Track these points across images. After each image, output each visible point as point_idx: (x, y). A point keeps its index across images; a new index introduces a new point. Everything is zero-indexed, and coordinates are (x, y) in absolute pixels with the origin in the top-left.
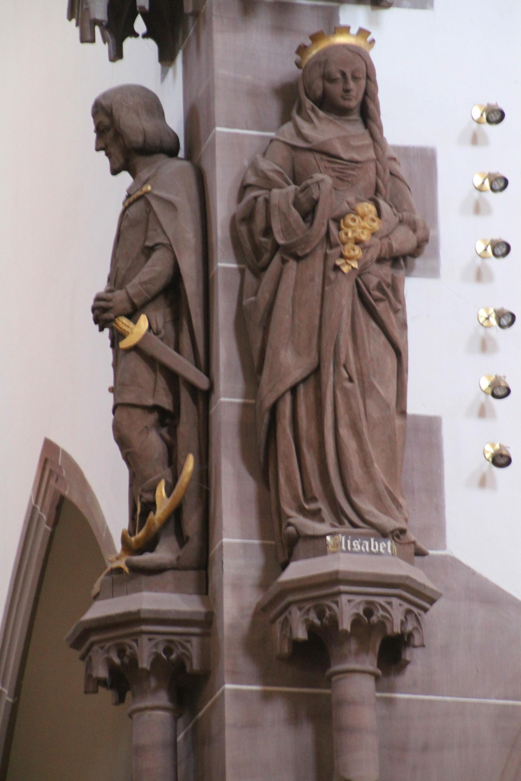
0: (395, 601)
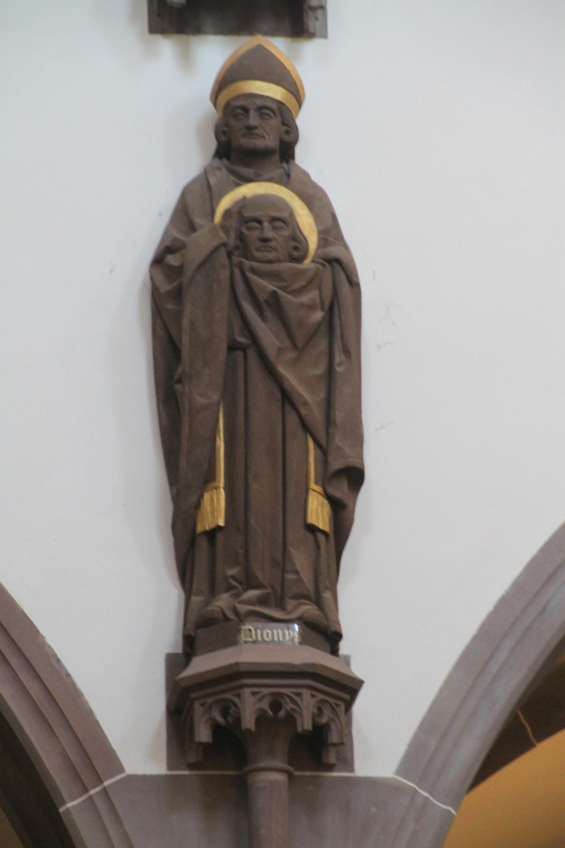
0: (306, 693)
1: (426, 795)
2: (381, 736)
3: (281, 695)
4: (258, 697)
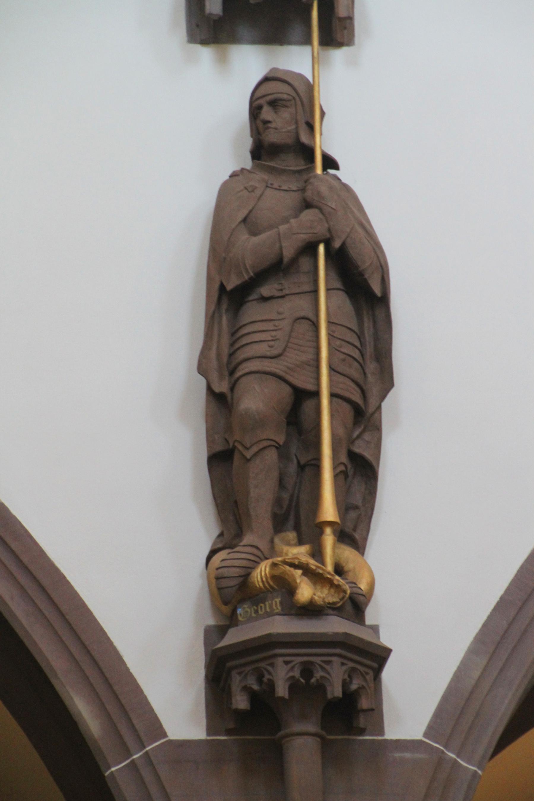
1: (454, 756)
2: (410, 701)
3: (312, 663)
4: (290, 665)
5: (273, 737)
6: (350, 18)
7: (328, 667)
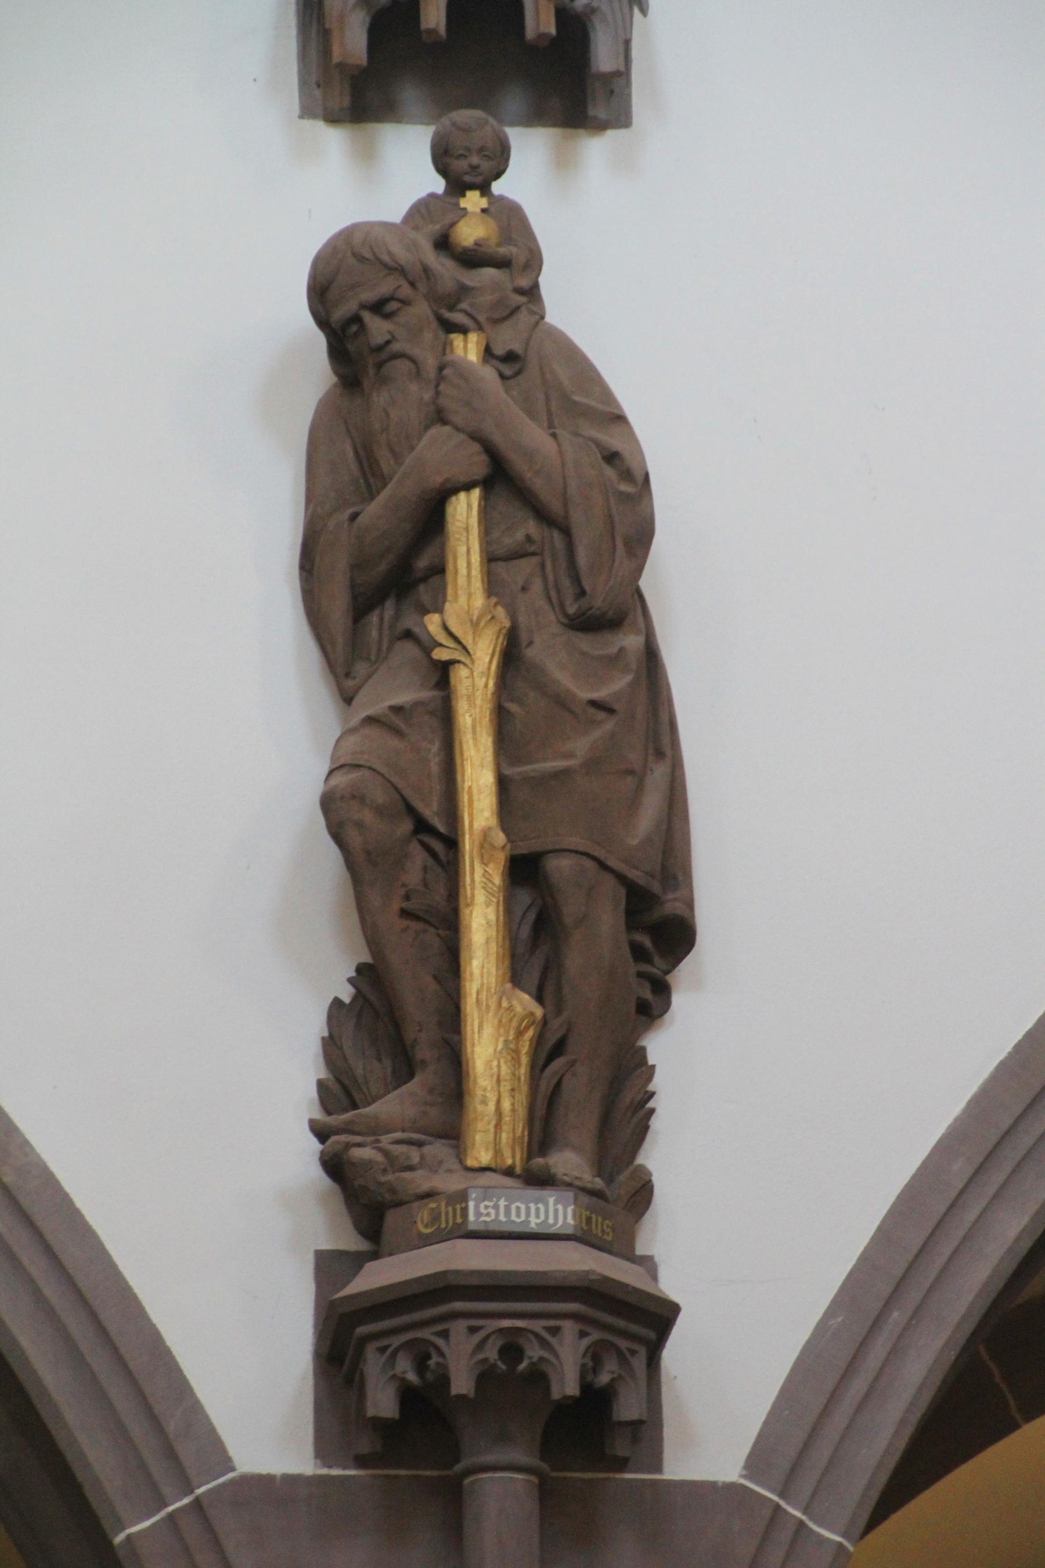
0: (569, 1327)
1: (798, 1514)
2: (719, 1401)
5: (445, 1473)
6: (622, 75)
7: (553, 1341)
